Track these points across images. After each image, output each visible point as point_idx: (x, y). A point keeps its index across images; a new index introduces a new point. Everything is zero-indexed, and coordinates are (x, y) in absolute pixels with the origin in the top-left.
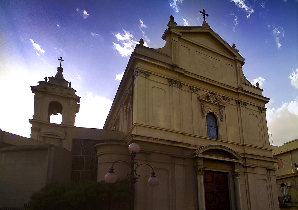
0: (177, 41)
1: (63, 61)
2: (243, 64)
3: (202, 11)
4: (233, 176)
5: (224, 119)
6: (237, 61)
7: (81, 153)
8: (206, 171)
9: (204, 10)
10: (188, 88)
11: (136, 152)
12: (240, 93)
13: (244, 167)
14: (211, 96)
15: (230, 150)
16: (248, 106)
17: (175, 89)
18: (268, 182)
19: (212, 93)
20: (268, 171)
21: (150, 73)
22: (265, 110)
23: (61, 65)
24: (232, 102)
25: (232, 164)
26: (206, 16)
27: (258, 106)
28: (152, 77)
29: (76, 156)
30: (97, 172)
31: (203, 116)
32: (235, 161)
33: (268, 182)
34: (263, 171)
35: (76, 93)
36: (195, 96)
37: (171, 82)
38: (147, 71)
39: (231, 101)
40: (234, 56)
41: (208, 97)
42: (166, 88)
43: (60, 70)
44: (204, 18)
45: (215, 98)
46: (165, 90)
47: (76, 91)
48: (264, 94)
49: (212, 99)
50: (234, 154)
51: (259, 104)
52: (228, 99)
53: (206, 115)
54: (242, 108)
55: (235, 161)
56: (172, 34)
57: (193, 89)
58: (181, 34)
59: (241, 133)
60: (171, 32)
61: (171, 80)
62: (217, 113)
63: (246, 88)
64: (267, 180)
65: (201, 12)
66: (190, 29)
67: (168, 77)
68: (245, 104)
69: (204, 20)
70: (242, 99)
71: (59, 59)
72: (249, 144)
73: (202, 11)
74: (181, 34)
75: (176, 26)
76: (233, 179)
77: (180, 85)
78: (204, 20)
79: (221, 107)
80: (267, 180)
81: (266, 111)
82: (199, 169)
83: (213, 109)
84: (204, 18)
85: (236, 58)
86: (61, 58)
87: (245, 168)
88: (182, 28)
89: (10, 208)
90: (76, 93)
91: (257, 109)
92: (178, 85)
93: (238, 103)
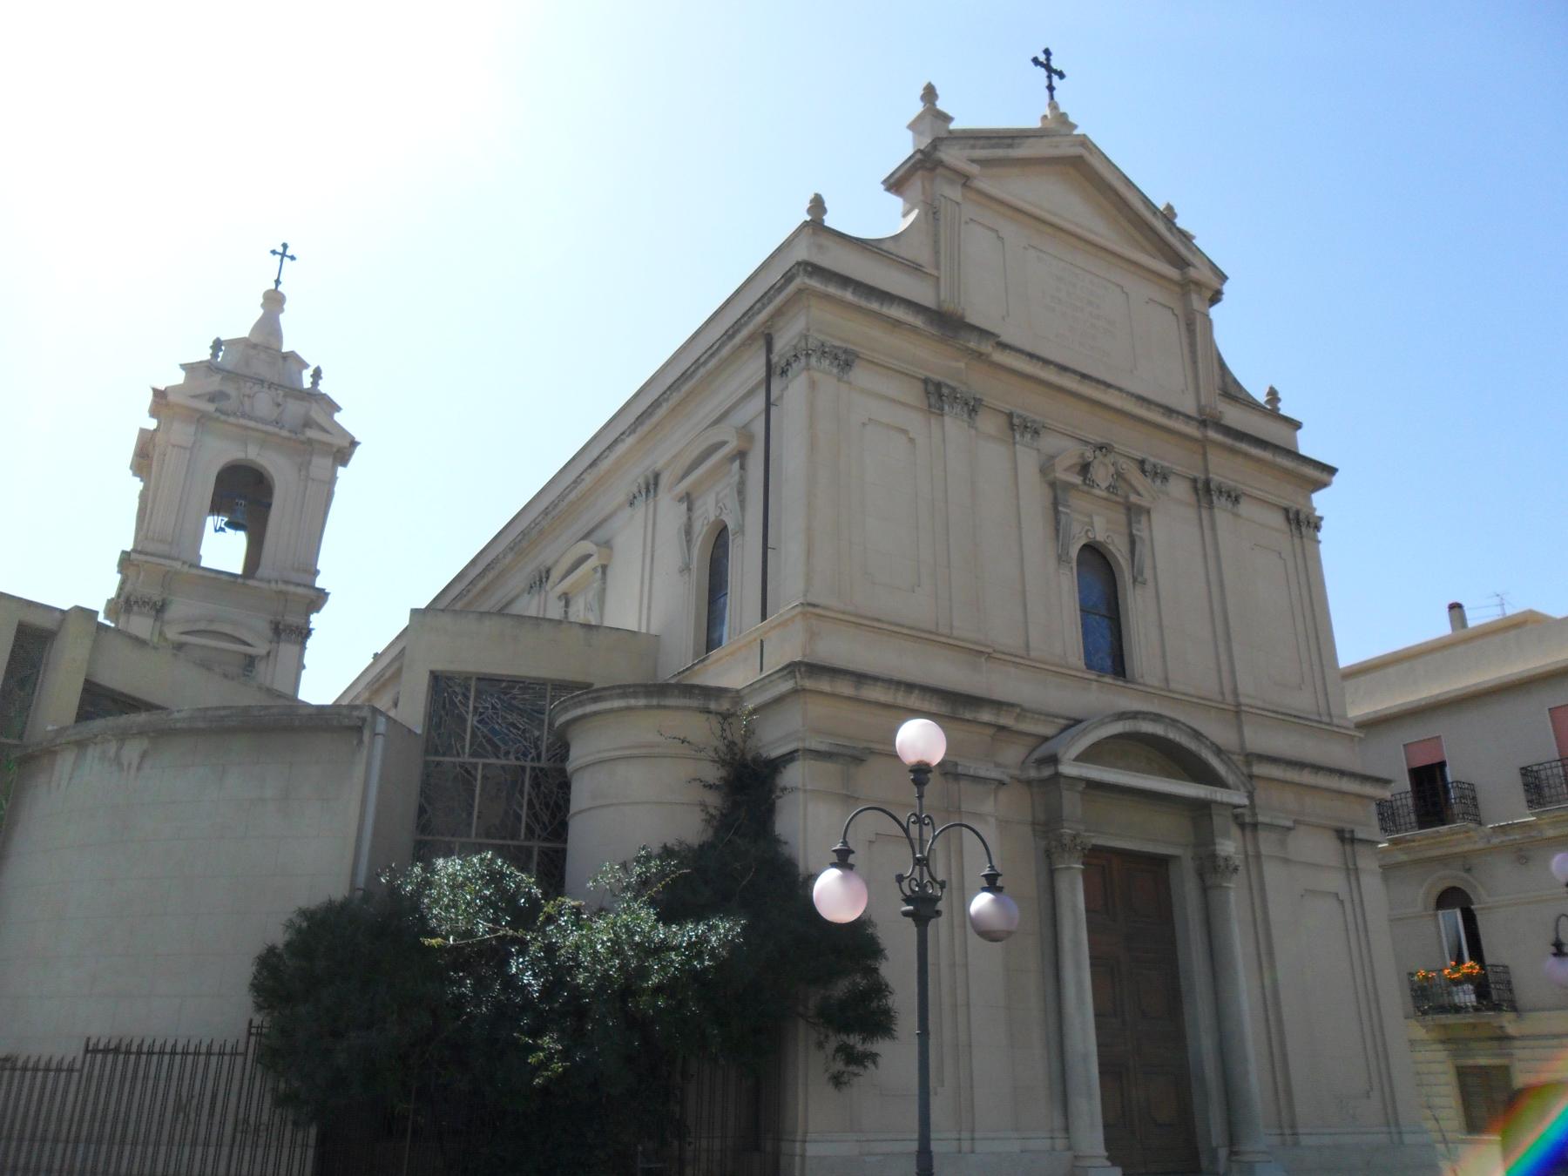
0: (958, 203)
1: (292, 258)
2: (1216, 298)
3: (1042, 58)
4: (1201, 875)
5: (1148, 574)
6: (1192, 287)
7: (463, 747)
8: (1097, 850)
9: (1047, 52)
10: (1002, 420)
11: (927, 765)
12: (1213, 442)
13: (1242, 826)
14: (1096, 463)
15: (1197, 735)
16: (1245, 507)
17: (954, 425)
18: (1348, 905)
19: (1101, 447)
20: (1348, 848)
21: (858, 357)
22: (1315, 524)
23: (278, 282)
24: (1179, 489)
25: (1201, 809)
26: (1055, 78)
27: (1285, 503)
28: (861, 375)
29: (438, 764)
30: (564, 851)
31: (1061, 559)
32: (1220, 795)
33: (1348, 905)
34: (1323, 848)
35: (337, 417)
36: (1028, 461)
37: (937, 395)
38: (844, 345)
39: (1173, 481)
40: (1181, 263)
41: (1085, 468)
42: (915, 422)
43: (274, 301)
44: (1051, 88)
45: (1112, 470)
46: (911, 435)
47: (338, 409)
48: (1307, 444)
49: (1102, 474)
50: (1215, 762)
51: (1287, 495)
52: (1161, 475)
53: (1074, 552)
54: (1222, 516)
55: (1220, 795)
56: (940, 170)
57: (1019, 427)
58: (974, 169)
59: (1222, 644)
60: (940, 163)
61: (938, 385)
62: (1118, 549)
63: (1233, 416)
64: (1344, 895)
65: (1036, 61)
66: (1010, 146)
67: (923, 374)
68: (1233, 495)
69: (1052, 97)
70: (1224, 469)
71: (274, 252)
72: (1260, 704)
73: (1042, 58)
74: (974, 169)
75: (950, 132)
76: (1205, 890)
77: (973, 407)
78: (1052, 97)
79: (1134, 512)
80: (1344, 895)
81: (1317, 528)
82: (1067, 840)
83: (1104, 527)
84: (1051, 88)
85: (1192, 272)
86: (285, 246)
87: (1248, 834)
88: (981, 142)
89: (150, 1041)
90: (337, 417)
91: (1277, 520)
92: (965, 409)
93: (1205, 491)
